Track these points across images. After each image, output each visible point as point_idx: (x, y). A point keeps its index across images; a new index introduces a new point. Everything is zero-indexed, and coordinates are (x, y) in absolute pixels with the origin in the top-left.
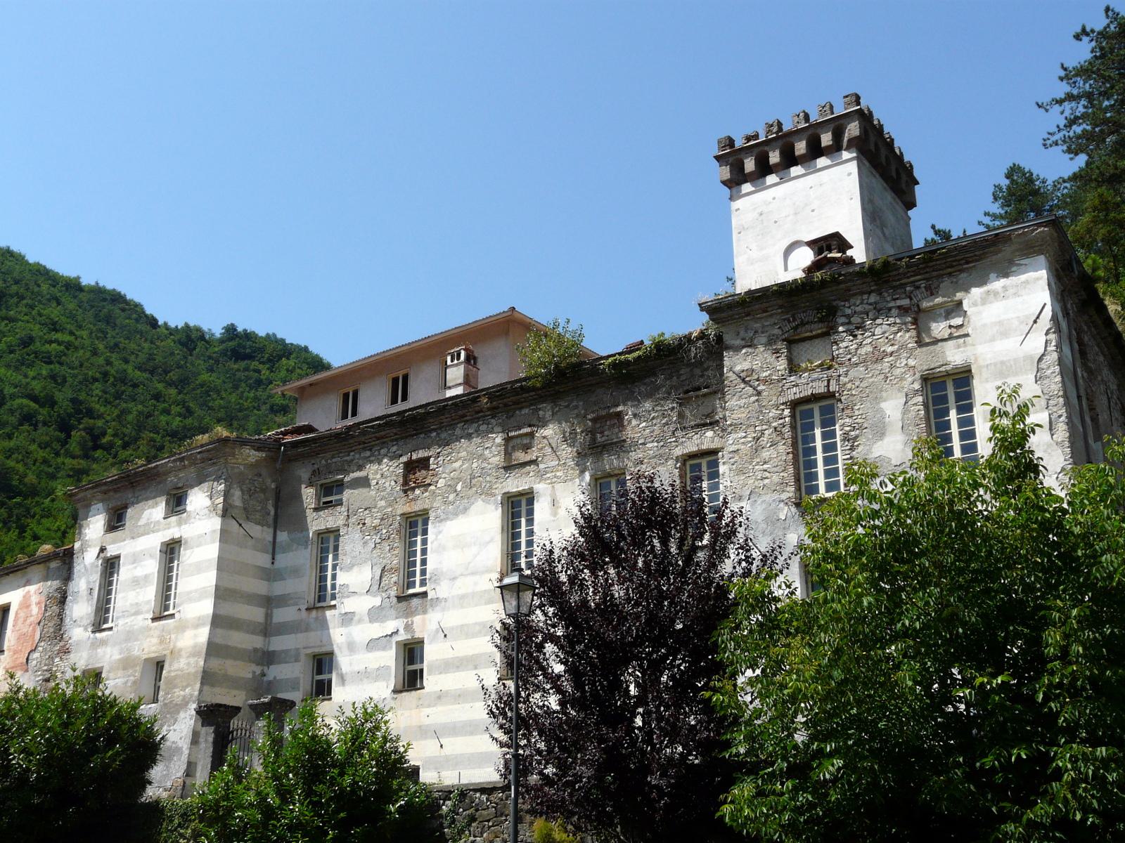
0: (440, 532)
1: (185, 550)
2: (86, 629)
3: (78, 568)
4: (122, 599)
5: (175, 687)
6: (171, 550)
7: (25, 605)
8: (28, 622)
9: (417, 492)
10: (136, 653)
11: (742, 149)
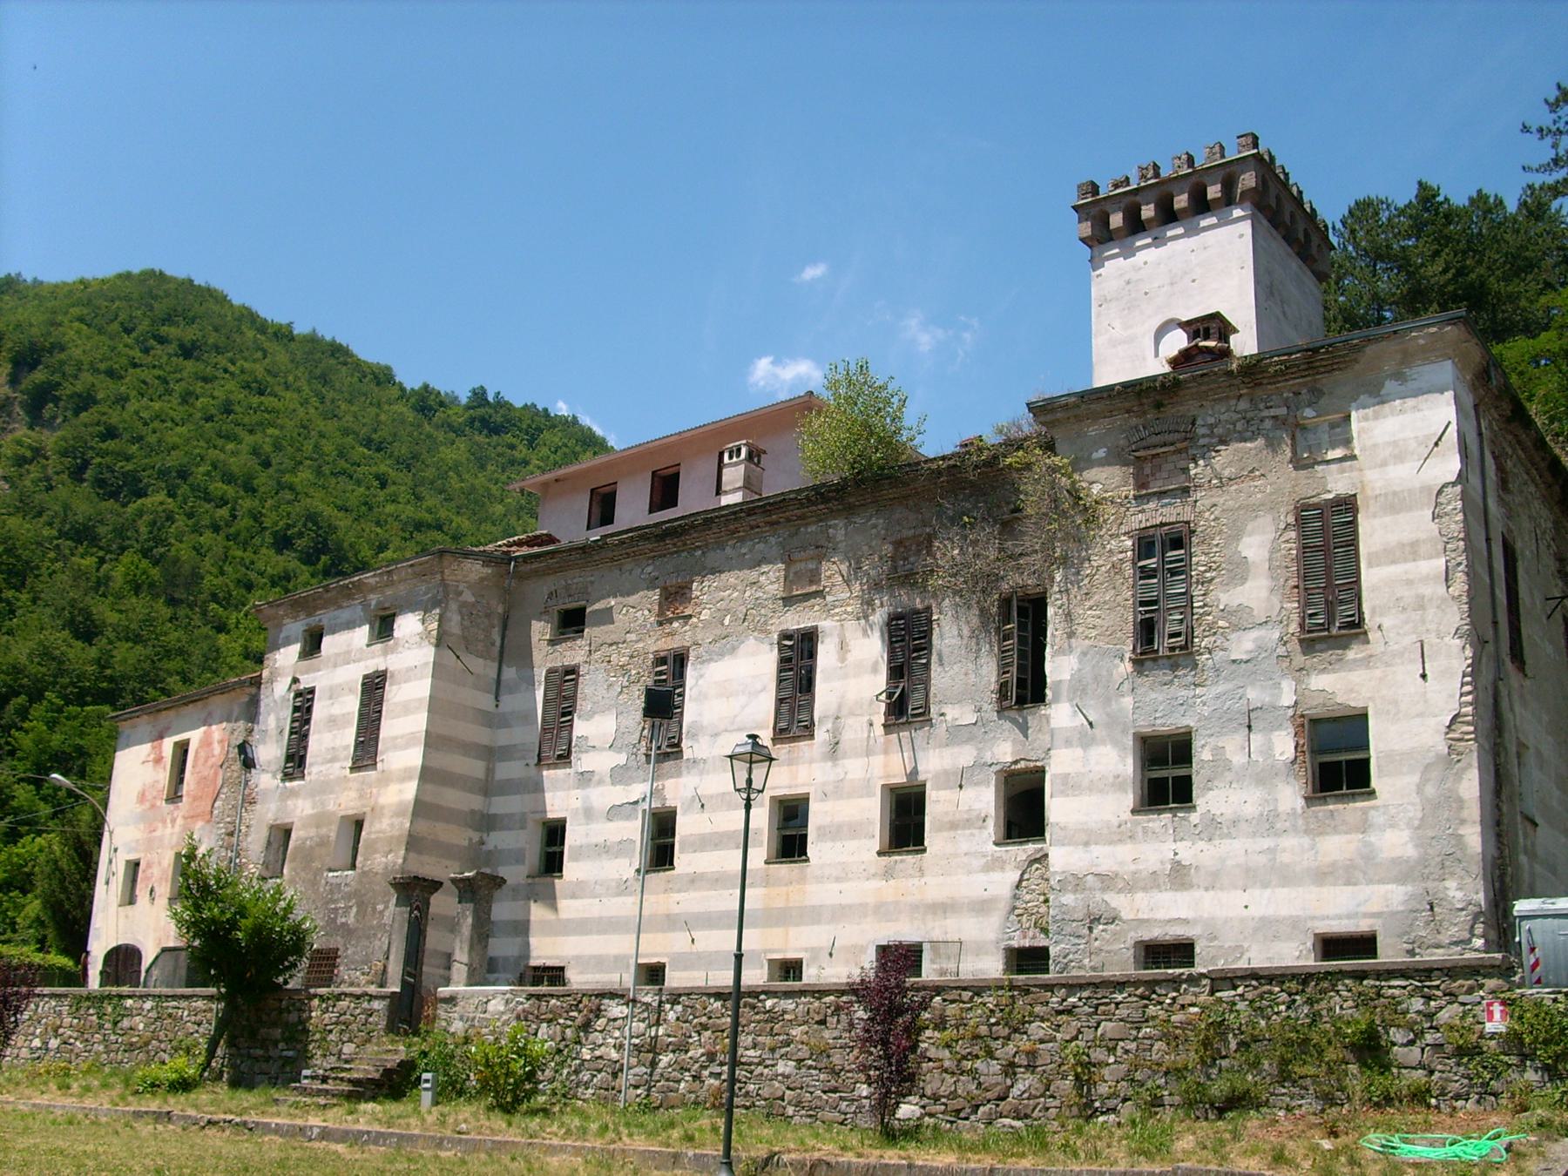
0: (701, 676)
1: (391, 685)
2: (274, 777)
3: (265, 702)
4: (318, 742)
5: (376, 851)
6: (374, 687)
7: (206, 742)
8: (210, 763)
9: (676, 625)
10: (331, 807)
11: (1170, 180)
